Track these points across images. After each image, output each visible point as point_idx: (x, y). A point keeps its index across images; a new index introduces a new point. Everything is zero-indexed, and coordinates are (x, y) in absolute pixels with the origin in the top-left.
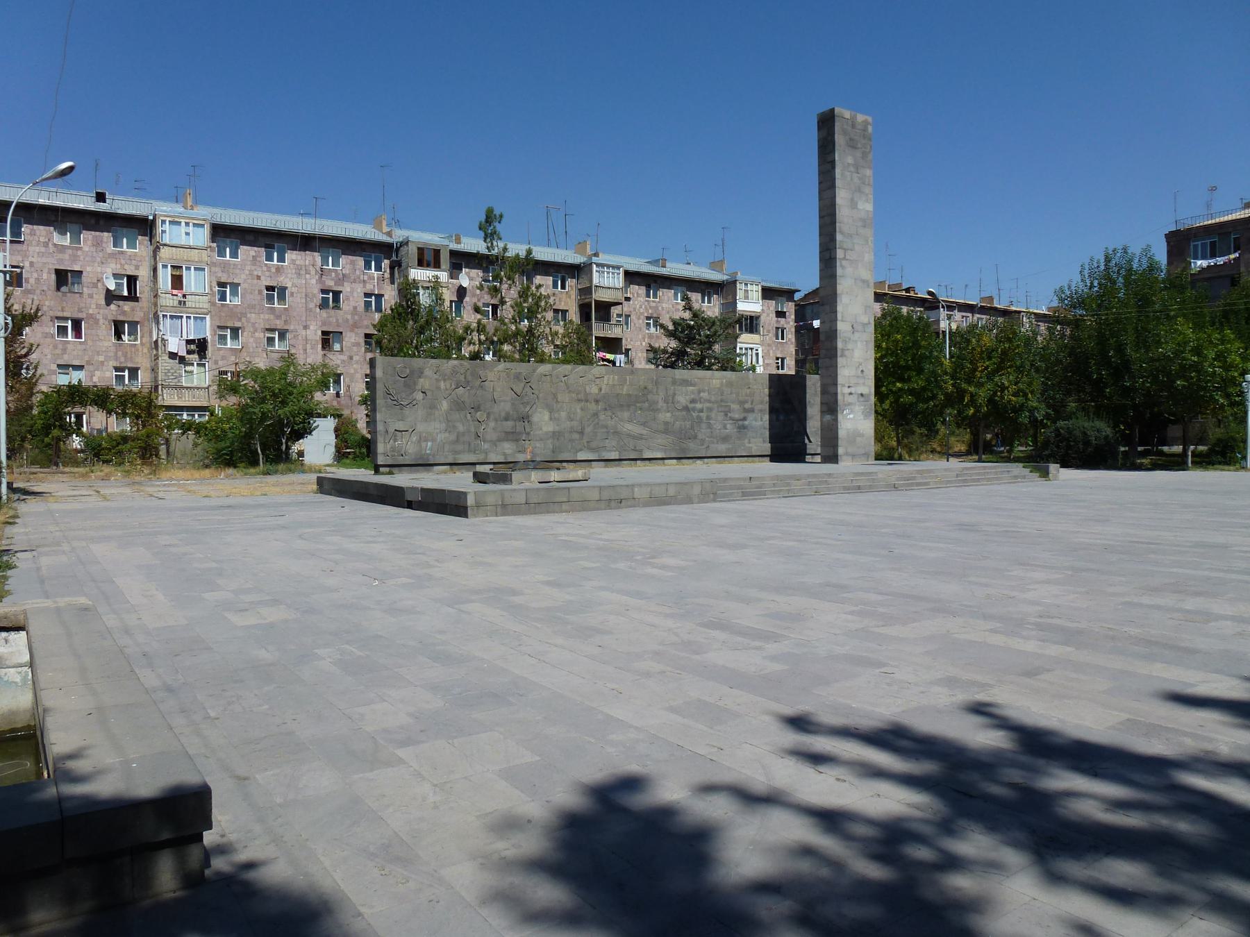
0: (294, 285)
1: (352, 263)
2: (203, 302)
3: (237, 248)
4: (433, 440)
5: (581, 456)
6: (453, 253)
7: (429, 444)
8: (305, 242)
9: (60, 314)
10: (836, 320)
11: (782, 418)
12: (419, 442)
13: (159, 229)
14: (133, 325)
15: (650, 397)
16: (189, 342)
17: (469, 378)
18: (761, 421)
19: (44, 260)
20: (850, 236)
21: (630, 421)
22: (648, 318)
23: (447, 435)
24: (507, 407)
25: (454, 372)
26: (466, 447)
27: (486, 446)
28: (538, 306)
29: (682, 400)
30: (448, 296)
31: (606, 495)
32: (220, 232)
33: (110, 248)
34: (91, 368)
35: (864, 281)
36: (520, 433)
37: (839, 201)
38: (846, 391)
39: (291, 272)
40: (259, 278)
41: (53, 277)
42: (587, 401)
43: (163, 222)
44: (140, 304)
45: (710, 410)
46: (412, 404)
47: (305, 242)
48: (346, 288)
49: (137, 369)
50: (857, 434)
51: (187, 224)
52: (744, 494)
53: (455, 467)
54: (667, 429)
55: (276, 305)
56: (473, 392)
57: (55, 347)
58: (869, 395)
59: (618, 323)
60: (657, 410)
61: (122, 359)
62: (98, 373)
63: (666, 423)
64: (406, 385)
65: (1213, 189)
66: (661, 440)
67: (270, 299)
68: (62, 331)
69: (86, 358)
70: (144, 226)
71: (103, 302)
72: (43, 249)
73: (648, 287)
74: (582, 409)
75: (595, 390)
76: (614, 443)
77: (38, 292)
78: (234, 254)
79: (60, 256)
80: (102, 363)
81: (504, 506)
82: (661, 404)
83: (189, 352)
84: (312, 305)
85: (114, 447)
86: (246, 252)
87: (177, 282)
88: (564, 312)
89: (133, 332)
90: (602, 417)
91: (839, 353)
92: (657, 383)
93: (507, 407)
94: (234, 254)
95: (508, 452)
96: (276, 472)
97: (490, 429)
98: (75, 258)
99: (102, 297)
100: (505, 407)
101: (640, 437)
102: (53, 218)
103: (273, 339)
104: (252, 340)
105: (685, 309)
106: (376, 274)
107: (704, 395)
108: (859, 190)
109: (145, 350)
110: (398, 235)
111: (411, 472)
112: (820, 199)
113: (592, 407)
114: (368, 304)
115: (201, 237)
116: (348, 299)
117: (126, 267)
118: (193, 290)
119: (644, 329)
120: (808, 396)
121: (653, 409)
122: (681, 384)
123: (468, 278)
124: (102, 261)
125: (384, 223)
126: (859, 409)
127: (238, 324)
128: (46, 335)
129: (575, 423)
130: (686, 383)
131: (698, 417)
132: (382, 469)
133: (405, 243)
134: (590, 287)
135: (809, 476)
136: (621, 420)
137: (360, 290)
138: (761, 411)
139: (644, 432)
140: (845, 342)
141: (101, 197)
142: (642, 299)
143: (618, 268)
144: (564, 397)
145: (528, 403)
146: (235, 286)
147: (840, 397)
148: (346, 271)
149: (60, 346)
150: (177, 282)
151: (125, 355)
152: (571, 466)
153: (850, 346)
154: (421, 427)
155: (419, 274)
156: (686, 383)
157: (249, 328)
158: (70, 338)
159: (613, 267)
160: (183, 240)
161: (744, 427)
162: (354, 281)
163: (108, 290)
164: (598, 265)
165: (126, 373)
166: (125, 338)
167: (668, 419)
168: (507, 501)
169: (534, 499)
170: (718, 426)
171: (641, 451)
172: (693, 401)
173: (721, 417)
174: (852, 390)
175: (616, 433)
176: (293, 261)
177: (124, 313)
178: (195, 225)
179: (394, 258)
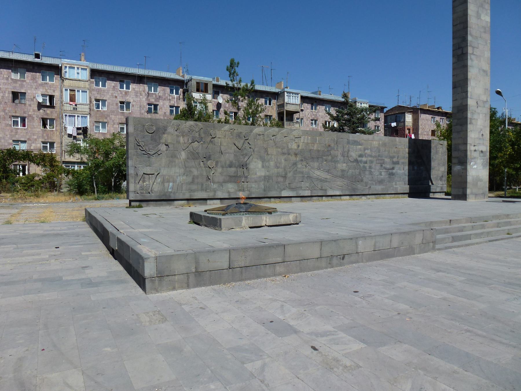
0: (134, 101)
1: (164, 90)
2: (86, 109)
3: (105, 82)
4: (174, 182)
5: (284, 194)
6: (215, 86)
7: (171, 184)
8: (140, 79)
9: (14, 114)
10: (467, 97)
11: (416, 168)
12: (163, 182)
13: (63, 71)
14: (52, 120)
15: (332, 152)
16: (78, 129)
17: (203, 135)
18: (403, 170)
19: (6, 87)
20: (476, 38)
21: (319, 169)
22: (312, 120)
23: (185, 177)
24: (231, 157)
25: (191, 130)
26: (200, 187)
27: (215, 186)
28: (257, 110)
29: (354, 155)
30: (211, 107)
31: (327, 251)
32: (95, 73)
33: (40, 81)
34: (30, 142)
35: (484, 71)
36: (240, 177)
37: (470, 12)
38: (473, 148)
39: (133, 94)
40: (116, 97)
41: (11, 95)
42: (289, 154)
43: (66, 67)
44: (55, 110)
45: (371, 162)
46: (158, 153)
47: (140, 79)
48: (160, 103)
49: (54, 143)
50: (478, 180)
51: (78, 68)
52: (454, 239)
53: (191, 202)
54: (343, 175)
55: (125, 111)
56: (205, 146)
57: (12, 131)
58: (486, 152)
59: (297, 122)
60: (336, 162)
61: (46, 138)
62: (33, 145)
63: (343, 171)
64: (152, 139)
66: (339, 182)
67: (122, 108)
68: (15, 123)
69: (28, 137)
70: (56, 70)
71: (37, 109)
72: (6, 81)
73: (312, 105)
74: (285, 160)
75: (294, 146)
76: (307, 185)
77: (3, 103)
78: (104, 85)
79: (14, 85)
80: (36, 139)
81: (198, 273)
82: (340, 157)
83: (78, 134)
84: (143, 111)
85: (29, 183)
86: (110, 84)
87: (72, 99)
88: (271, 116)
89: (52, 124)
90: (299, 166)
91: (468, 122)
92: (337, 143)
93: (231, 157)
94: (104, 85)
95: (232, 190)
96: (103, 198)
97: (218, 174)
98: (22, 86)
99: (36, 106)
100: (229, 157)
101: (325, 180)
102: (11, 66)
103: (123, 128)
104: (112, 129)
106: (176, 96)
107: (368, 152)
108: (482, 6)
109: (58, 133)
110: (187, 77)
111: (156, 206)
112: (454, 12)
113: (293, 158)
114: (172, 111)
115: (85, 75)
116: (161, 108)
117: (48, 91)
118: (81, 102)
119: (310, 125)
120: (432, 154)
121: (334, 160)
122: (353, 144)
123: (221, 99)
124: (36, 88)
125: (181, 71)
126: (480, 161)
127: (105, 121)
128: (7, 125)
129: (280, 170)
130: (356, 143)
131: (364, 167)
132: (133, 204)
133: (191, 80)
134: (284, 104)
135: (497, 217)
136: (313, 168)
137: (167, 104)
138: (403, 163)
139: (328, 177)
140: (473, 113)
141: (37, 56)
142: (309, 110)
143: (298, 94)
144: (273, 151)
145: (246, 155)
146: (104, 101)
147: (469, 153)
148: (161, 94)
149: (14, 131)
150: (72, 99)
151: (47, 135)
152: (277, 200)
153: (475, 116)
154: (164, 172)
155: (197, 96)
156: (356, 143)
157: (111, 123)
158: (19, 127)
159: (295, 94)
160: (76, 77)
161: (393, 174)
162: (165, 99)
163: (39, 102)
164: (288, 92)
165: (48, 145)
166: (48, 127)
167: (344, 168)
168: (203, 267)
169: (240, 261)
170: (376, 173)
171: (326, 190)
173: (378, 167)
174: (476, 148)
175: (309, 177)
176: (134, 89)
177: (47, 114)
178: (82, 69)
179: (185, 88)
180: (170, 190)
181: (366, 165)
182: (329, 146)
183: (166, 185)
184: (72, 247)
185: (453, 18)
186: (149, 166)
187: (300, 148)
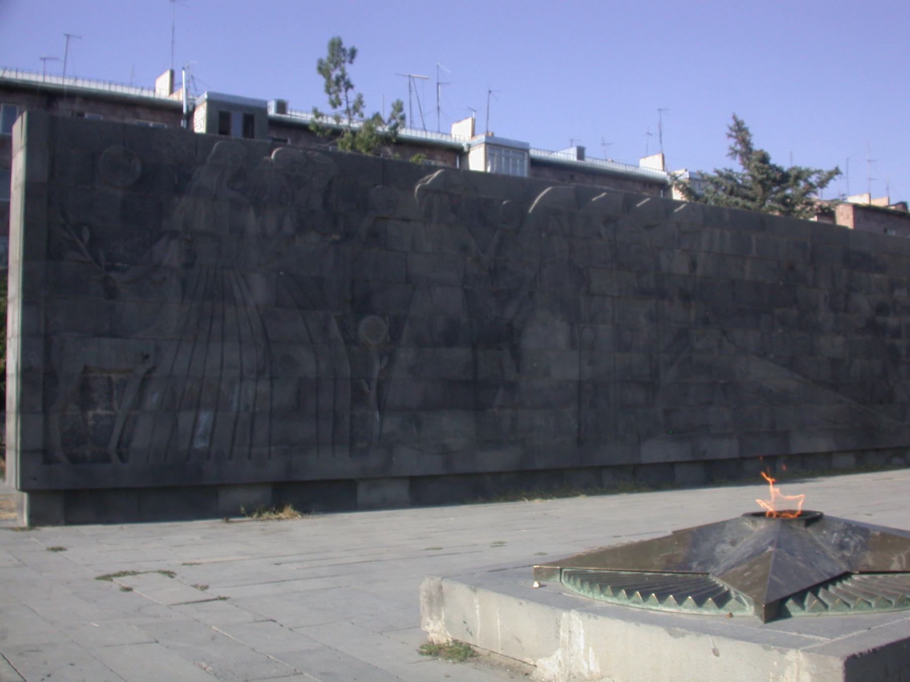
7: (205, 417)
23: (264, 387)
105: (664, 170)
107: (900, 294)
172: (881, 309)
180: (200, 445)
181: (898, 342)
182: (791, 268)
183: (185, 419)
185: (5, 358)
186: (112, 335)
187: (699, 272)
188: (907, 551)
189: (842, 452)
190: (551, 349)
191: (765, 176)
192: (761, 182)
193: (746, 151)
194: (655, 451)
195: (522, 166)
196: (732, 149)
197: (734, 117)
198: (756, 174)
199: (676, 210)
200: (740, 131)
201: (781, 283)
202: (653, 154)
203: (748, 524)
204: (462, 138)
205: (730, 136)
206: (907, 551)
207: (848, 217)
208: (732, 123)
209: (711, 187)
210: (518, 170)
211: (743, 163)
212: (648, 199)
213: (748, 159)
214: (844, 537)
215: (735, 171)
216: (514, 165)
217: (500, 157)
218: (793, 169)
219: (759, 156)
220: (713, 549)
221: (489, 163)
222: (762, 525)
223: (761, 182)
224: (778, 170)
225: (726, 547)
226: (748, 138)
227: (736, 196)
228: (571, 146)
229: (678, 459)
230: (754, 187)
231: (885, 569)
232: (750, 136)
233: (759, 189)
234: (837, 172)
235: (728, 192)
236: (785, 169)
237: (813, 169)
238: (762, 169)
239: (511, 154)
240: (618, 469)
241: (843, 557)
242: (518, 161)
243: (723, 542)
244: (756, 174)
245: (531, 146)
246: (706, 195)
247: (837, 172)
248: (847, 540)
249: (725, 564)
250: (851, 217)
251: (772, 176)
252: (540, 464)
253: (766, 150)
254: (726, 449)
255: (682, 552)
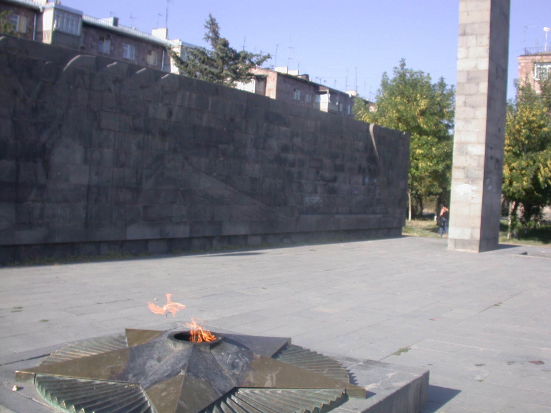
42: (148, 132)
63: (254, 180)
65: (526, 27)
107: (297, 141)
172: (285, 149)
181: (293, 170)
182: (232, 120)
184: (106, 391)
187: (173, 119)
188: (277, 372)
189: (254, 235)
190: (72, 166)
191: (224, 55)
192: (222, 58)
193: (215, 37)
194: (136, 232)
195: (77, 26)
196: (206, 35)
197: (210, 16)
198: (219, 53)
199: (162, 78)
200: (213, 25)
201: (225, 129)
202: (161, 28)
203: (170, 344)
204: (40, 2)
205: (206, 27)
206: (277, 372)
207: (274, 80)
208: (208, 19)
209: (191, 57)
210: (74, 28)
211: (213, 45)
212: (144, 69)
213: (216, 42)
214: (236, 359)
215: (207, 49)
216: (72, 25)
217: (63, 18)
218: (243, 52)
219: (222, 42)
220: (145, 364)
221: (55, 22)
222: (180, 347)
223: (222, 58)
224: (233, 51)
225: (153, 362)
226: (217, 30)
227: (207, 64)
228: (110, 16)
229: (151, 237)
230: (217, 60)
231: (262, 386)
232: (218, 28)
233: (220, 62)
234: (269, 57)
235: (201, 61)
236: (238, 52)
237: (254, 53)
238: (224, 50)
239: (70, 17)
240: (111, 243)
241: (234, 374)
242: (75, 23)
243: (152, 358)
244: (219, 53)
245: (84, 13)
246: (188, 62)
247: (269, 57)
248: (237, 361)
249: (151, 378)
250: (276, 79)
251: (229, 55)
252: (58, 239)
253: (227, 39)
254: (182, 232)
255: (122, 365)
